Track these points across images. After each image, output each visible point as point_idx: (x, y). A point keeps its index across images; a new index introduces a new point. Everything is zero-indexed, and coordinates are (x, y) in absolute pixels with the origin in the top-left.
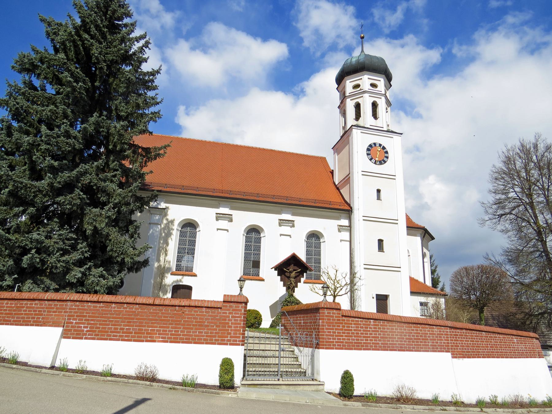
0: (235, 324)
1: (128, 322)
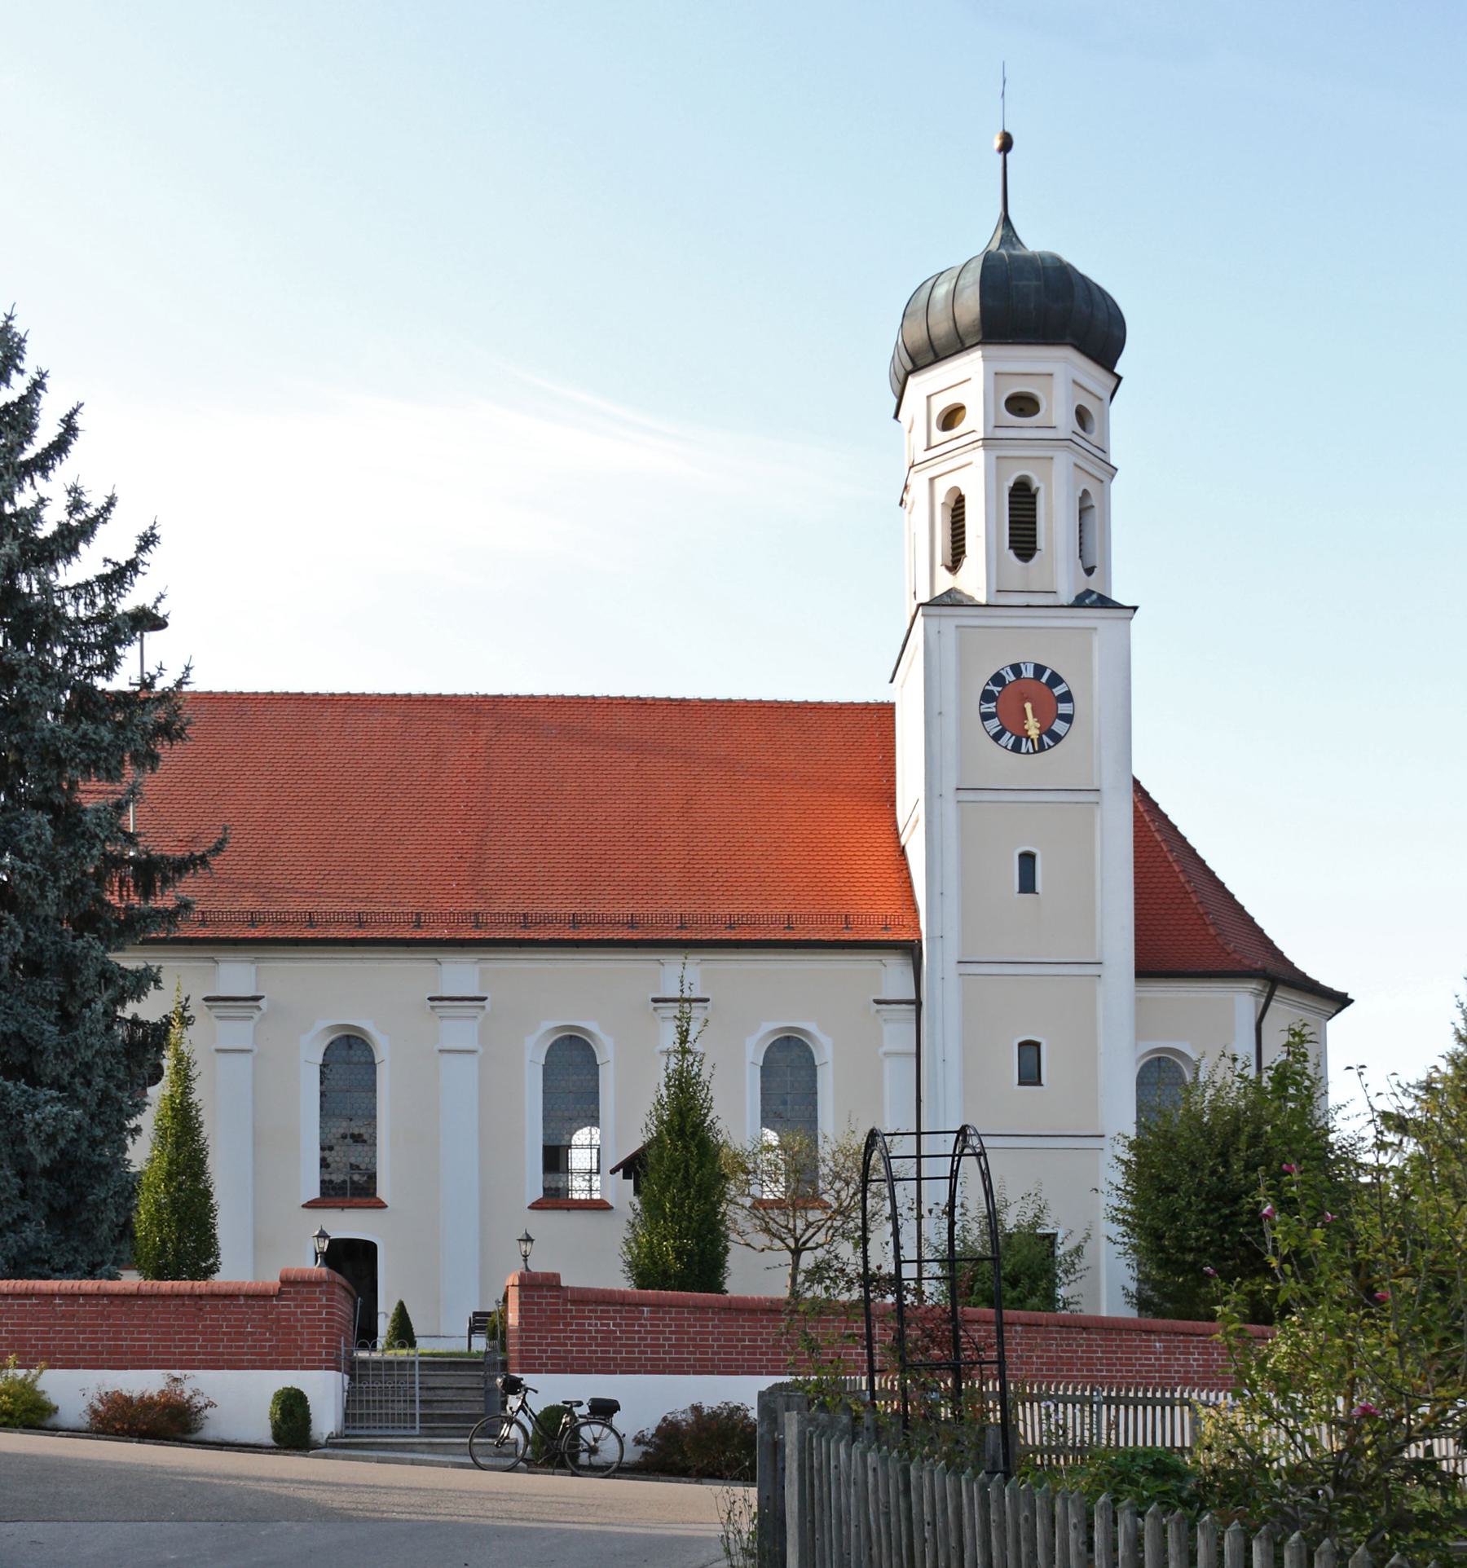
0: (309, 1327)
1: (92, 1332)
